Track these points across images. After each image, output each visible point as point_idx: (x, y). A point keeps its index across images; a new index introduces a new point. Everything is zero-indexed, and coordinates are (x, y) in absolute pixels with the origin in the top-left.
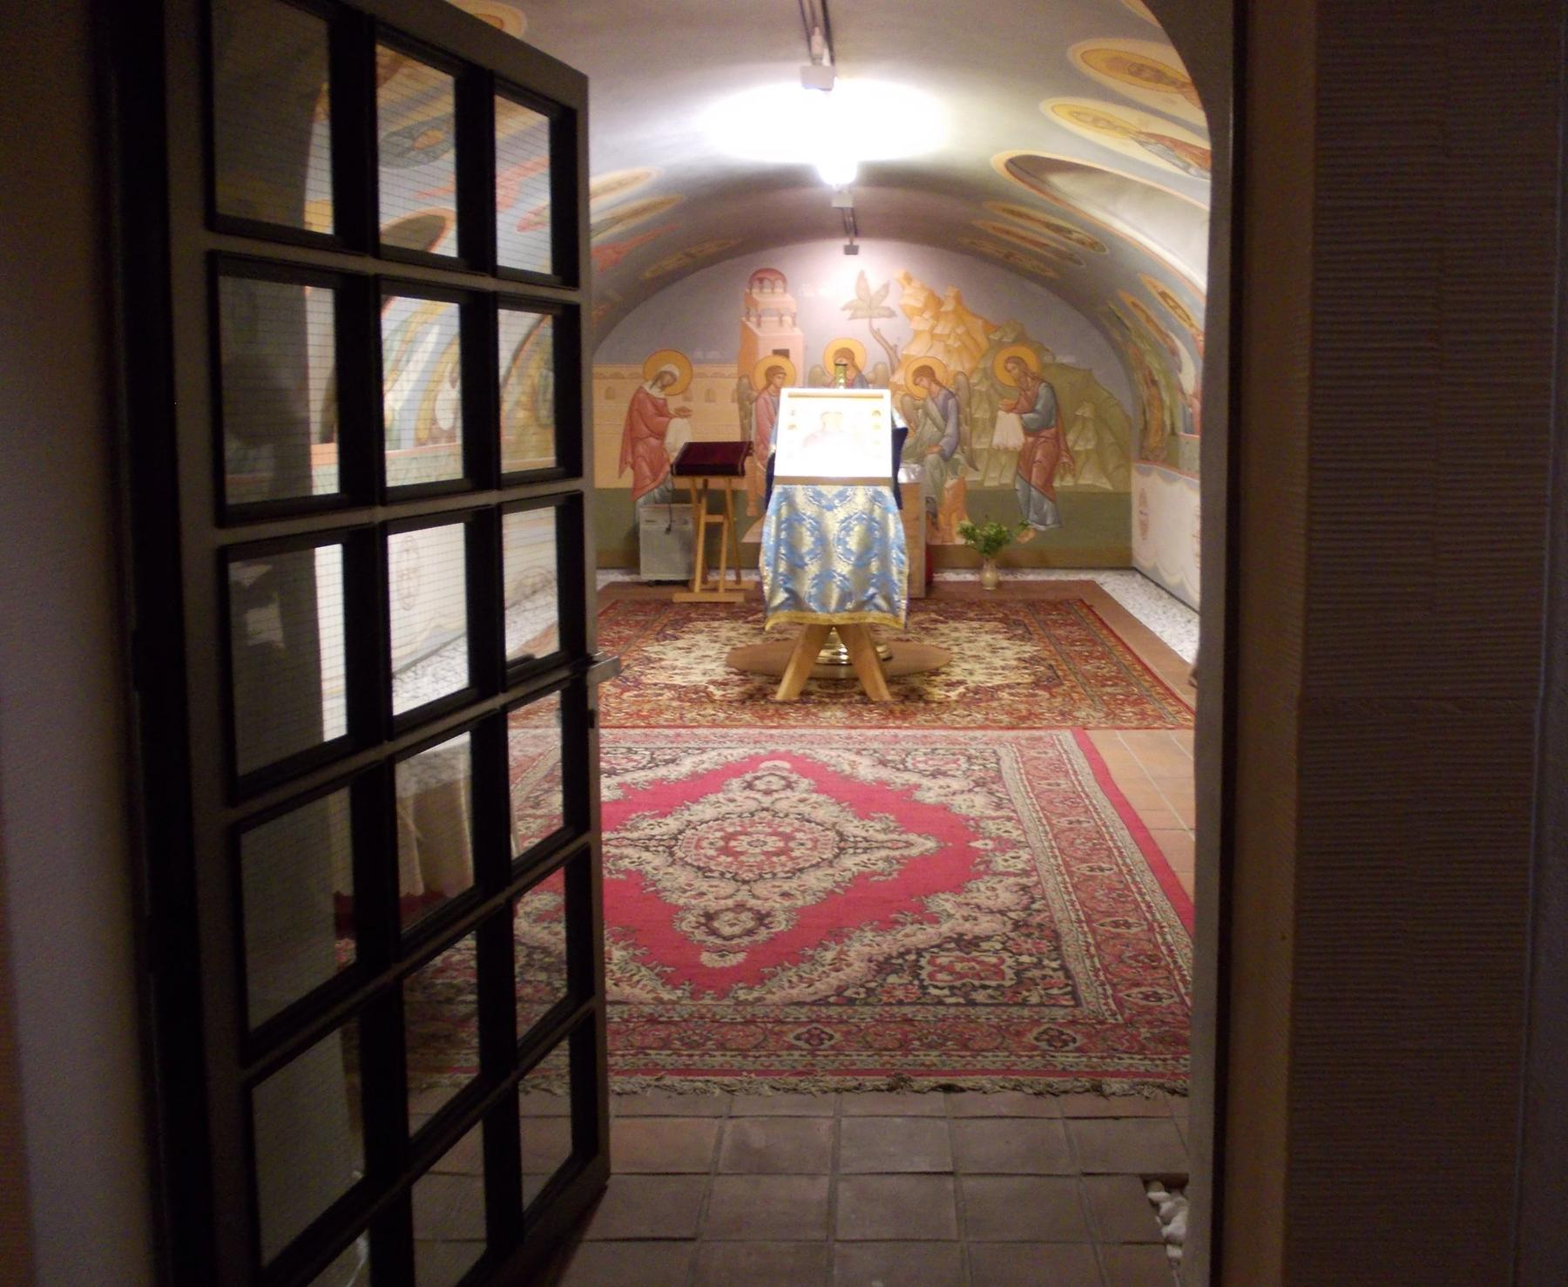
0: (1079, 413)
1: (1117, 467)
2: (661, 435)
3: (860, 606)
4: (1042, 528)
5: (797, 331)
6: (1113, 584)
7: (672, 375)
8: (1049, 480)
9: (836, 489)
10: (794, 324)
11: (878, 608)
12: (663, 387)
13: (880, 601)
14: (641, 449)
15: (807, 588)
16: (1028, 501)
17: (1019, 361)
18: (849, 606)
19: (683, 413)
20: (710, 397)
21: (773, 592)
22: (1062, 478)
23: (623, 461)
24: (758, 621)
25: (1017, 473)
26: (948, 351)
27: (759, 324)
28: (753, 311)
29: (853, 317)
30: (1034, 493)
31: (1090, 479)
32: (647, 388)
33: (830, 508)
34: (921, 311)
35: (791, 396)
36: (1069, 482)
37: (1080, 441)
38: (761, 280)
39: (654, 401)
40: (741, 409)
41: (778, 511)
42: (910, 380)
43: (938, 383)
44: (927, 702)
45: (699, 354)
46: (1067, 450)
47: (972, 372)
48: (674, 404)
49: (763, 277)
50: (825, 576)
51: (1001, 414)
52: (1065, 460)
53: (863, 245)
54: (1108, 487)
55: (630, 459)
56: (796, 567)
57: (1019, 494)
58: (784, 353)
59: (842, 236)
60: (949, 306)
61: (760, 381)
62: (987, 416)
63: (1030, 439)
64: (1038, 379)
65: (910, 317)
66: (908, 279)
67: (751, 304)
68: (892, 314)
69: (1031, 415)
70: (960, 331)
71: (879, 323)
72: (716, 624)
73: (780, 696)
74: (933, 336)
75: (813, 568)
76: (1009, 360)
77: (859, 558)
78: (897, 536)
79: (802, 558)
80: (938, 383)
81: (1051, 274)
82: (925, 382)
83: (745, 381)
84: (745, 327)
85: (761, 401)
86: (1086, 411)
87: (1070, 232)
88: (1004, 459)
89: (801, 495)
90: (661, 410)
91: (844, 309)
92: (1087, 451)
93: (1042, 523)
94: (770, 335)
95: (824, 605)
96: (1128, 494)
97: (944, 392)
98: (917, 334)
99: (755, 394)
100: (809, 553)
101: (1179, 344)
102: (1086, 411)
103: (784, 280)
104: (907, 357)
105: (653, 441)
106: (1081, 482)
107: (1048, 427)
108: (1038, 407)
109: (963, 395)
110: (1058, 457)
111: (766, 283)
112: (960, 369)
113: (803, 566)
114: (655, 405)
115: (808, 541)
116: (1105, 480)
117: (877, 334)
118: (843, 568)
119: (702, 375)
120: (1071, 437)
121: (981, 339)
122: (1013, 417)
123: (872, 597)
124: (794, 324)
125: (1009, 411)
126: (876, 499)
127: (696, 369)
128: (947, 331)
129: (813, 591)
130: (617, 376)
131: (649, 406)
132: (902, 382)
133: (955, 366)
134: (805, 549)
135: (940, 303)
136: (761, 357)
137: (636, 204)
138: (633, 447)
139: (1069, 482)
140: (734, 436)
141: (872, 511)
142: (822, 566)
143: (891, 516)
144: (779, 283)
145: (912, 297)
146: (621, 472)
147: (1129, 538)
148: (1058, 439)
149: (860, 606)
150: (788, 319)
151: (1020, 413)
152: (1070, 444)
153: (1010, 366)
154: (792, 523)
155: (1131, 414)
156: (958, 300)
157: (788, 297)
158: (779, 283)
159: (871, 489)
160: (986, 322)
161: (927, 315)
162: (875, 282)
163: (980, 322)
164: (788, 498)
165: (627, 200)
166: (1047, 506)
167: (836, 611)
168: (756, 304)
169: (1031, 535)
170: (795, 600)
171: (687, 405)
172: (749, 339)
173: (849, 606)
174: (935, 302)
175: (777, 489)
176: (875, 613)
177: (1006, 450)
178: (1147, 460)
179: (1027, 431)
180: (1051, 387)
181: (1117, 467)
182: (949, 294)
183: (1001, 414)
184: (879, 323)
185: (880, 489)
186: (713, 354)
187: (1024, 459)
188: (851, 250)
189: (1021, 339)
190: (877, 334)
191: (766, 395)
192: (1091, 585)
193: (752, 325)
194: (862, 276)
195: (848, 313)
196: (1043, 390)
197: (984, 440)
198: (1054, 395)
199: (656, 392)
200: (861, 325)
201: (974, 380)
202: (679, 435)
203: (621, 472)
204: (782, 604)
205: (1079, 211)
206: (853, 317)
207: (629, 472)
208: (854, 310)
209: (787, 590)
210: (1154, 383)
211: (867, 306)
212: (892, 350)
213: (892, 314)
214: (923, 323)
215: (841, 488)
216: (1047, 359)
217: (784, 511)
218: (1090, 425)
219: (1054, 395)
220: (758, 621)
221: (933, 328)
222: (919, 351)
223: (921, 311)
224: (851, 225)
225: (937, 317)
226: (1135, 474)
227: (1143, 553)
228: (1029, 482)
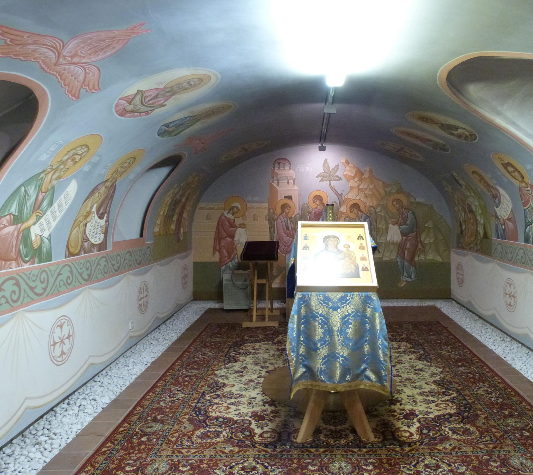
0: (427, 225)
1: (445, 251)
2: (232, 237)
3: (356, 377)
4: (410, 280)
5: (296, 187)
6: (446, 308)
7: (237, 208)
8: (413, 257)
9: (340, 295)
10: (294, 184)
11: (368, 378)
12: (233, 214)
13: (369, 373)
14: (223, 244)
15: (319, 365)
16: (403, 268)
17: (399, 201)
18: (348, 378)
19: (243, 226)
20: (255, 218)
21: (296, 371)
22: (419, 256)
23: (215, 249)
24: (279, 343)
25: (398, 253)
26: (366, 196)
27: (278, 184)
28: (275, 178)
29: (322, 181)
30: (406, 263)
31: (431, 256)
32: (226, 214)
33: (335, 309)
34: (354, 178)
35: (303, 226)
36: (422, 258)
37: (427, 239)
38: (279, 164)
39: (229, 220)
40: (270, 224)
41: (299, 312)
42: (348, 209)
43: (362, 212)
44: (402, 444)
45: (250, 198)
46: (421, 243)
47: (378, 205)
48: (238, 221)
49: (281, 161)
50: (331, 357)
51: (391, 226)
52: (420, 247)
53: (328, 147)
54: (441, 260)
55: (218, 248)
56: (312, 349)
57: (399, 264)
58: (290, 198)
59: (317, 142)
60: (366, 175)
61: (279, 211)
62: (384, 227)
63: (404, 238)
64: (408, 209)
65: (349, 181)
66: (347, 162)
67: (274, 175)
68: (340, 179)
69: (404, 226)
70: (371, 187)
71: (333, 183)
72: (257, 345)
73: (300, 438)
74: (359, 189)
75: (323, 351)
76: (394, 201)
77: (356, 343)
78: (381, 329)
79: (315, 344)
80: (362, 212)
81: (421, 158)
82: (355, 211)
83: (272, 210)
84: (271, 184)
85: (279, 220)
86: (430, 224)
87: (456, 128)
88: (392, 247)
89: (314, 302)
90: (232, 225)
91: (318, 177)
92: (430, 243)
93: (410, 277)
94: (284, 189)
95: (331, 378)
96: (450, 263)
97: (364, 215)
98: (352, 188)
99: (276, 217)
100: (321, 339)
101: (501, 191)
102: (430, 224)
103: (290, 164)
104: (347, 199)
105: (229, 239)
106: (428, 258)
107: (412, 232)
108: (408, 223)
109: (373, 216)
110: (417, 246)
111: (281, 164)
112: (371, 205)
113: (316, 349)
114: (230, 223)
115: (319, 332)
116: (439, 257)
117: (333, 188)
118: (342, 351)
119: (251, 208)
120: (423, 237)
121: (382, 191)
122: (396, 227)
123: (365, 369)
124: (294, 184)
125: (394, 224)
126: (366, 301)
127: (249, 205)
128: (365, 187)
129: (323, 367)
130: (210, 209)
131: (227, 223)
132: (345, 211)
133: (369, 203)
134: (317, 338)
135: (362, 174)
136: (279, 199)
137: (207, 106)
138: (220, 243)
139: (422, 258)
140: (266, 238)
141: (364, 310)
142: (330, 350)
143: (377, 314)
144: (287, 165)
145: (349, 171)
146: (214, 254)
147: (449, 284)
148: (417, 237)
149: (356, 377)
150: (291, 181)
151: (399, 226)
152: (422, 240)
153: (395, 203)
154: (308, 318)
155: (450, 226)
156: (371, 172)
157: (292, 171)
158: (287, 165)
159: (364, 294)
160: (383, 183)
161: (356, 179)
162: (332, 165)
163: (381, 183)
164: (305, 302)
165: (198, 102)
166: (412, 269)
167: (339, 382)
168: (277, 174)
169: (404, 283)
170: (310, 372)
171: (245, 222)
172: (273, 191)
173: (348, 378)
174: (360, 173)
175: (298, 295)
176: (366, 381)
177: (393, 243)
178: (463, 248)
179: (403, 234)
180: (413, 213)
181: (445, 251)
182: (366, 169)
183: (391, 226)
184: (333, 183)
185: (369, 294)
186: (256, 198)
187: (401, 247)
188: (322, 149)
189: (400, 191)
190: (333, 188)
191: (281, 217)
192: (434, 308)
193: (274, 184)
194: (326, 160)
195: (320, 179)
196: (410, 214)
197: (383, 238)
198: (415, 217)
199: (230, 216)
200: (326, 184)
201: (378, 210)
202: (242, 238)
203: (214, 254)
204: (301, 376)
205: (476, 112)
206: (322, 181)
207: (217, 254)
208: (322, 177)
209: (305, 366)
210: (471, 211)
211: (328, 175)
212: (340, 196)
213: (340, 179)
214: (354, 183)
215: (343, 294)
216: (412, 200)
217: (303, 311)
218: (432, 231)
219: (415, 217)
220: (279, 343)
221: (359, 186)
222: (352, 196)
223: (354, 178)
224: (323, 133)
225: (361, 180)
226: (453, 255)
227: (456, 290)
228: (404, 259)
